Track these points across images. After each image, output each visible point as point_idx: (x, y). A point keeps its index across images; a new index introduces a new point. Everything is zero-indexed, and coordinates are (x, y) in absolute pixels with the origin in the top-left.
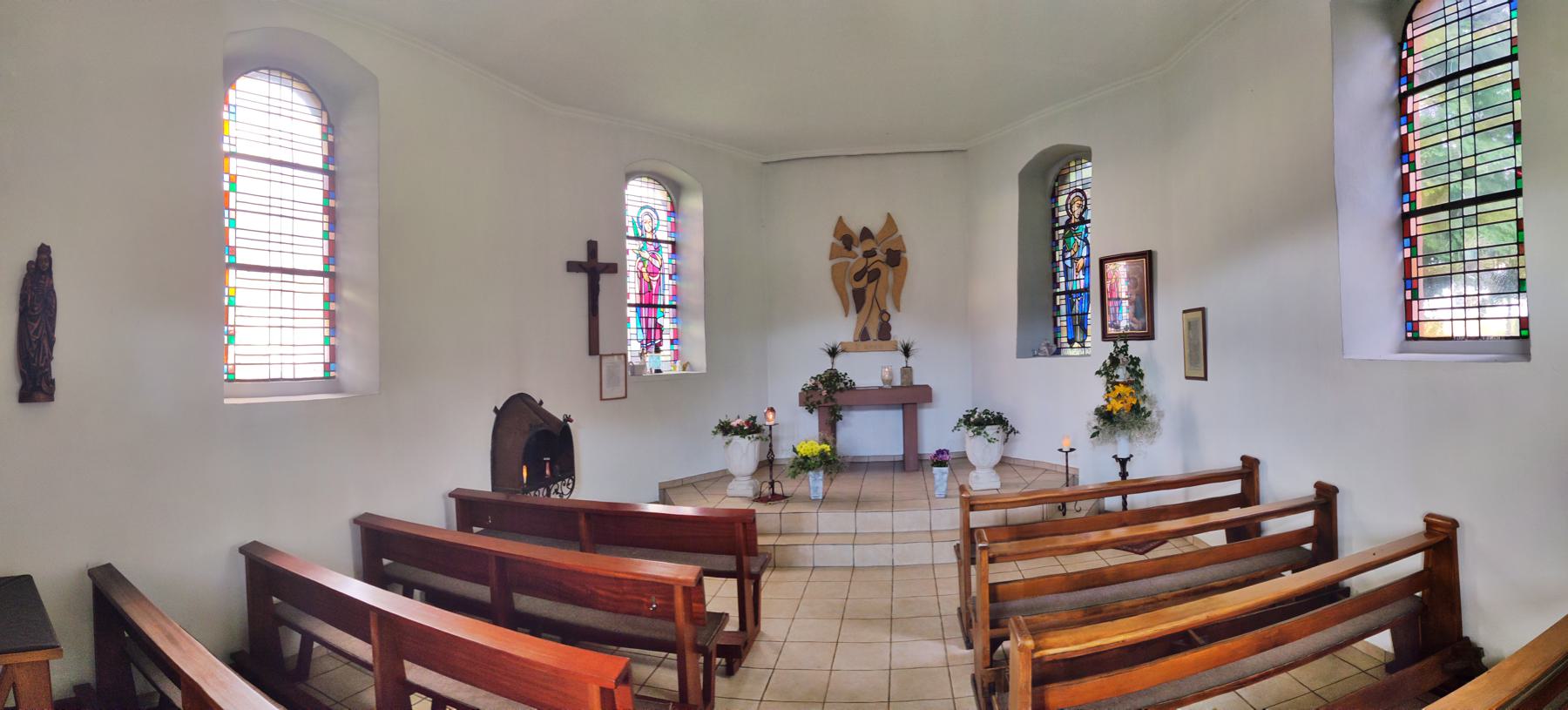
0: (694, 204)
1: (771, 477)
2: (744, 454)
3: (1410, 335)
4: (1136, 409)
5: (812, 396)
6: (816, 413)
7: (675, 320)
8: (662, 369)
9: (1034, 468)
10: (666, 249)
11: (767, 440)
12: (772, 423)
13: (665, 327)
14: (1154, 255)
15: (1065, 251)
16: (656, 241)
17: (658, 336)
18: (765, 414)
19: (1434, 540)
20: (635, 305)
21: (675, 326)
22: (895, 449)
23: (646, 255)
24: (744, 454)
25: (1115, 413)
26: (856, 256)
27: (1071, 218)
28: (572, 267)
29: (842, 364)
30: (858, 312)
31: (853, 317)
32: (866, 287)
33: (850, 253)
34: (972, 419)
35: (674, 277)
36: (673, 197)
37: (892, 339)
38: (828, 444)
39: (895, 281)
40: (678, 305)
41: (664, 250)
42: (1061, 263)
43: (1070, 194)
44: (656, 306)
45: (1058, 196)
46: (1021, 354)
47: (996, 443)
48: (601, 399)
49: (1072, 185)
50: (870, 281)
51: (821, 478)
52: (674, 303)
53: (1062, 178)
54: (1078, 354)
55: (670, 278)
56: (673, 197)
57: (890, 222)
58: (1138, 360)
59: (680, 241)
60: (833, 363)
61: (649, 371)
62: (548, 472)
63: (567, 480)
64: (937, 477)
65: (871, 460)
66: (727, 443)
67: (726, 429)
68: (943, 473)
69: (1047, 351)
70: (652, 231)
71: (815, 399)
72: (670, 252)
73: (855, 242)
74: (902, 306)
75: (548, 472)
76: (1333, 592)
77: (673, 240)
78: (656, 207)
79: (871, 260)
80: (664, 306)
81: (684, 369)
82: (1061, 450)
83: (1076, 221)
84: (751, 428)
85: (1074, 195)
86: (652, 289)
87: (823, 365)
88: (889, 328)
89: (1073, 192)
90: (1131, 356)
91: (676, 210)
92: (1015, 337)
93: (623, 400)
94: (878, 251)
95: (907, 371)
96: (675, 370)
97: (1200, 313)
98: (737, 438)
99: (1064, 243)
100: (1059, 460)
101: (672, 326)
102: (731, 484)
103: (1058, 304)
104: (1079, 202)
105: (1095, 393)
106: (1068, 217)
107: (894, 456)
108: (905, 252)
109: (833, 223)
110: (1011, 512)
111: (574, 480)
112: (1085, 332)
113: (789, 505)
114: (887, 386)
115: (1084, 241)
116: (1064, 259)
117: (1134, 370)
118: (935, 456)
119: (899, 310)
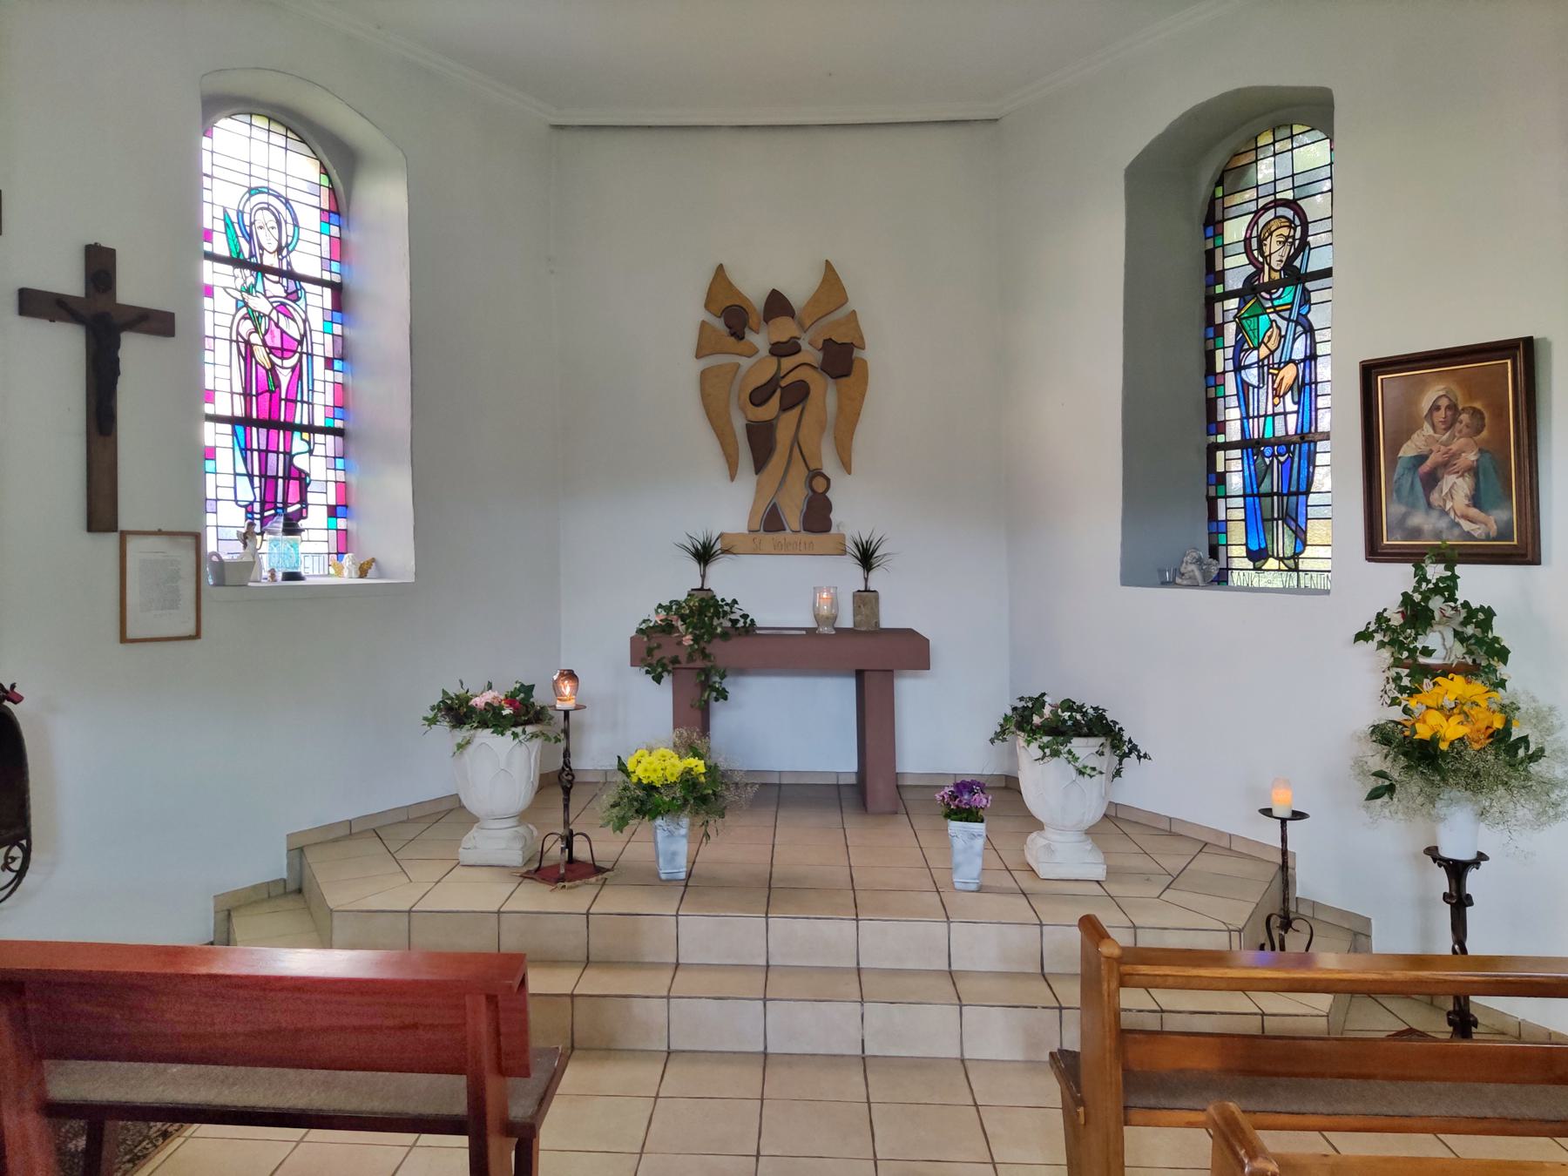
1: (566, 823)
5: (659, 646)
6: (667, 680)
7: (340, 463)
8: (302, 571)
9: (1171, 834)
10: (318, 300)
11: (558, 740)
12: (569, 705)
15: (1239, 348)
16: (290, 275)
17: (294, 494)
18: (555, 683)
20: (232, 421)
21: (341, 476)
22: (842, 761)
23: (260, 304)
26: (753, 352)
27: (1260, 271)
28: (33, 303)
29: (725, 580)
32: (777, 417)
33: (741, 346)
34: (1036, 720)
35: (338, 365)
36: (333, 172)
37: (834, 530)
38: (701, 757)
39: (840, 408)
40: (350, 427)
42: (1230, 377)
43: (1258, 213)
44: (290, 427)
46: (1133, 575)
47: (1098, 777)
48: (124, 639)
49: (1262, 191)
50: (785, 408)
51: (683, 831)
52: (339, 424)
53: (1232, 175)
54: (1278, 584)
55: (329, 364)
57: (831, 280)
58: (1489, 613)
59: (354, 282)
60: (703, 577)
61: (265, 574)
64: (958, 844)
65: (785, 781)
66: (460, 747)
67: (457, 712)
68: (973, 836)
69: (1197, 574)
70: (279, 250)
71: (667, 652)
72: (328, 305)
73: (753, 320)
77: (336, 279)
78: (291, 195)
79: (788, 363)
80: (311, 429)
81: (363, 573)
82: (1267, 812)
83: (1276, 276)
85: (1270, 215)
86: (278, 386)
87: (682, 579)
88: (828, 506)
89: (1266, 208)
90: (1466, 605)
91: (343, 208)
92: (1119, 539)
93: (188, 643)
95: (866, 599)
96: (339, 573)
98: (485, 736)
99: (1240, 329)
100: (1269, 834)
101: (331, 475)
103: (1220, 468)
104: (1285, 231)
106: (1251, 269)
108: (863, 348)
111: (27, 852)
112: (1300, 536)
113: (606, 891)
114: (825, 630)
115: (1297, 323)
116: (1239, 368)
117: (1480, 642)
119: (849, 473)
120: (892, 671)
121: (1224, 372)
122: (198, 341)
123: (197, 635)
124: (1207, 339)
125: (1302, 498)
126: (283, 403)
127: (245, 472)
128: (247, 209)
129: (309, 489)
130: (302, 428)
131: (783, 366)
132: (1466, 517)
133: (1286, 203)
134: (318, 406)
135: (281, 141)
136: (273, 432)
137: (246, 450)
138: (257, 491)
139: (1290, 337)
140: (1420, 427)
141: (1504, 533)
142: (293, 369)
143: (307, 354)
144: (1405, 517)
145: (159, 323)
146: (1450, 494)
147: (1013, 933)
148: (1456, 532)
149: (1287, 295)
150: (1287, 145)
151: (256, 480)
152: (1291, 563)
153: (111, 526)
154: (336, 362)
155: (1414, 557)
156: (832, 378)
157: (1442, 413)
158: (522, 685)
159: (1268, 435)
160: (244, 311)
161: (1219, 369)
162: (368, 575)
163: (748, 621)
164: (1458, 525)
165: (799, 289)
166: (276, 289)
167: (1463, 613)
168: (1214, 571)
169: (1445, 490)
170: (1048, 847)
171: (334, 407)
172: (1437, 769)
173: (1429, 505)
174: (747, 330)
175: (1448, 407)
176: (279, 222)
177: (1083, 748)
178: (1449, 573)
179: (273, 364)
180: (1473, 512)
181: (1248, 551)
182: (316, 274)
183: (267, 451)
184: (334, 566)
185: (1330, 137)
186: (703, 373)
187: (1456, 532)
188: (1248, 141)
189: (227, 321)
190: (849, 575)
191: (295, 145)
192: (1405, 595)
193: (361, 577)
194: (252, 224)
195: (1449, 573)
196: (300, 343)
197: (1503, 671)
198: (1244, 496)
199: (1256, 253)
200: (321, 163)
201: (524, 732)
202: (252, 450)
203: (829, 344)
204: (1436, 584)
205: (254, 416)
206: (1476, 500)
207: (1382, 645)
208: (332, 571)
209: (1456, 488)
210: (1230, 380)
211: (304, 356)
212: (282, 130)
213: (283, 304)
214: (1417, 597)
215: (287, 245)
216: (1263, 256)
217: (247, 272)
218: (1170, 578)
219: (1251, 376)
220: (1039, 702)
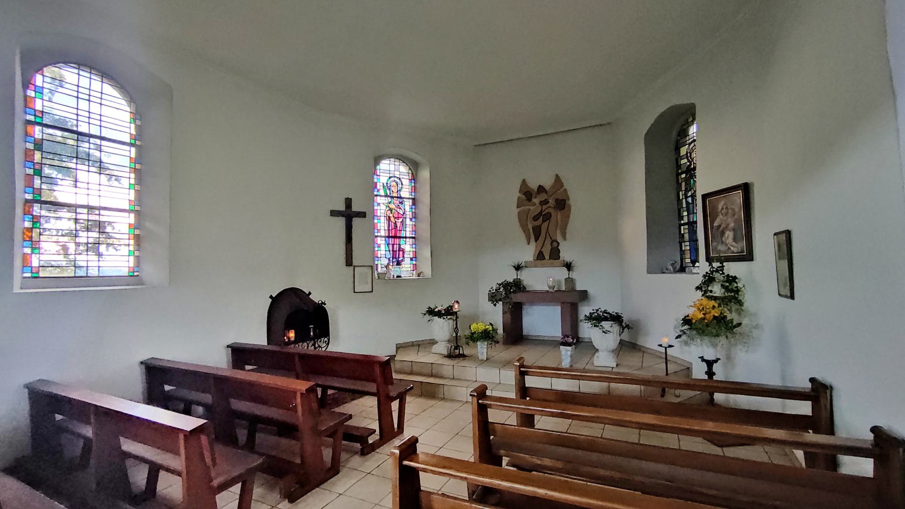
0: (425, 174)
2: (441, 329)
10: (408, 204)
13: (406, 250)
15: (687, 191)
16: (400, 198)
21: (414, 250)
24: (441, 329)
25: (694, 321)
27: (691, 164)
28: (334, 213)
30: (536, 241)
31: (533, 243)
35: (414, 220)
41: (406, 203)
42: (684, 200)
44: (400, 237)
46: (652, 269)
50: (543, 221)
52: (414, 236)
55: (411, 219)
56: (413, 171)
62: (312, 334)
64: (563, 353)
66: (429, 321)
67: (431, 312)
68: (567, 350)
69: (672, 269)
75: (312, 334)
78: (401, 177)
79: (544, 207)
80: (406, 237)
82: (660, 345)
84: (449, 312)
86: (396, 227)
95: (570, 281)
96: (413, 276)
103: (682, 232)
108: (569, 200)
110: (613, 385)
111: (329, 339)
114: (551, 290)
116: (686, 197)
121: (682, 199)
122: (374, 216)
126: (398, 232)
128: (389, 182)
130: (403, 237)
132: (732, 246)
136: (395, 239)
137: (388, 244)
142: (401, 222)
145: (362, 215)
151: (391, 252)
153: (351, 265)
160: (388, 208)
164: (729, 248)
165: (548, 183)
166: (397, 201)
169: (726, 236)
173: (723, 242)
175: (726, 208)
176: (397, 184)
178: (721, 265)
179: (396, 222)
180: (734, 244)
182: (408, 197)
183: (394, 244)
189: (383, 211)
190: (563, 273)
194: (390, 186)
195: (721, 265)
196: (403, 215)
198: (689, 241)
199: (689, 158)
201: (447, 318)
203: (557, 200)
204: (717, 269)
206: (735, 240)
212: (398, 160)
213: (399, 206)
216: (691, 158)
217: (389, 198)
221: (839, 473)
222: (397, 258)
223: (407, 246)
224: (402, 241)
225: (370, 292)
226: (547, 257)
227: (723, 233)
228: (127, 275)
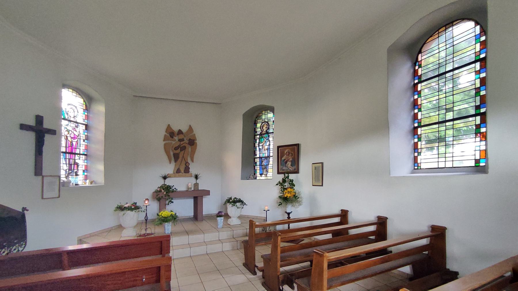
0: (100, 109)
3: (416, 168)
4: (295, 196)
10: (82, 128)
14: (300, 145)
15: (259, 143)
19: (434, 234)
21: (86, 164)
23: (69, 128)
27: (262, 132)
28: (23, 127)
29: (169, 182)
32: (180, 153)
34: (231, 201)
35: (86, 141)
40: (88, 154)
44: (75, 154)
45: (257, 124)
48: (42, 198)
52: (86, 153)
53: (258, 117)
55: (84, 141)
57: (191, 129)
58: (293, 180)
59: (91, 123)
63: (22, 243)
64: (219, 221)
67: (121, 208)
68: (222, 219)
69: (253, 178)
70: (74, 117)
72: (84, 129)
74: (194, 160)
76: (383, 251)
77: (86, 123)
79: (182, 143)
80: (80, 154)
81: (91, 183)
82: (265, 210)
83: (265, 133)
85: (264, 123)
86: (73, 145)
87: (161, 182)
89: (263, 122)
90: (290, 179)
94: (185, 139)
95: (196, 185)
96: (85, 183)
97: (321, 164)
98: (129, 212)
99: (259, 140)
101: (84, 164)
102: (123, 231)
103: (256, 161)
104: (266, 126)
105: (275, 192)
107: (190, 216)
108: (196, 140)
109: (165, 127)
111: (26, 243)
112: (267, 171)
116: (259, 146)
117: (292, 184)
118: (218, 214)
119: (193, 162)
120: (203, 196)
122: (61, 136)
123: (59, 197)
124: (254, 141)
125: (268, 166)
126: (74, 149)
127: (65, 163)
129: (79, 167)
130: (78, 154)
131: (181, 143)
132: (291, 168)
133: (266, 122)
134: (82, 149)
135: (75, 94)
136: (71, 155)
138: (68, 167)
139: (266, 142)
140: (285, 155)
141: (295, 170)
142: (76, 142)
143: (79, 139)
144: (283, 168)
145: (53, 132)
146: (288, 165)
147: (229, 232)
148: (289, 170)
149: (266, 135)
150: (267, 113)
151: (68, 165)
152: (266, 175)
154: (86, 141)
155: (284, 173)
156: (190, 145)
157: (288, 153)
158: (134, 203)
159: (263, 156)
160: (66, 129)
161: (256, 146)
162: (93, 184)
163: (176, 189)
164: (289, 169)
165: (184, 129)
166: (73, 125)
167: (290, 181)
168: (255, 177)
170: (232, 220)
171: (85, 150)
172: (288, 201)
173: (286, 166)
174: (174, 136)
176: (74, 111)
177: (238, 204)
179: (72, 141)
180: (291, 167)
181: (260, 174)
183: (70, 159)
184: (84, 182)
185: (273, 113)
186: (165, 144)
187: (289, 170)
188: (261, 112)
190: (193, 181)
191: (78, 95)
192: (283, 178)
193: (91, 184)
196: (78, 136)
197: (294, 188)
198: (259, 165)
200: (84, 100)
202: (67, 159)
205: (68, 151)
206: (291, 165)
207: (280, 185)
208: (84, 183)
209: (289, 164)
210: (258, 148)
211: (79, 139)
213: (74, 128)
214: (284, 178)
215: (76, 116)
216: (263, 129)
218: (248, 178)
219: (261, 147)
220: (231, 198)
221: (350, 234)
222: (73, 169)
223: (81, 161)
224: (77, 157)
225: (58, 198)
226: (183, 172)
227: (286, 162)
228: (474, 165)
